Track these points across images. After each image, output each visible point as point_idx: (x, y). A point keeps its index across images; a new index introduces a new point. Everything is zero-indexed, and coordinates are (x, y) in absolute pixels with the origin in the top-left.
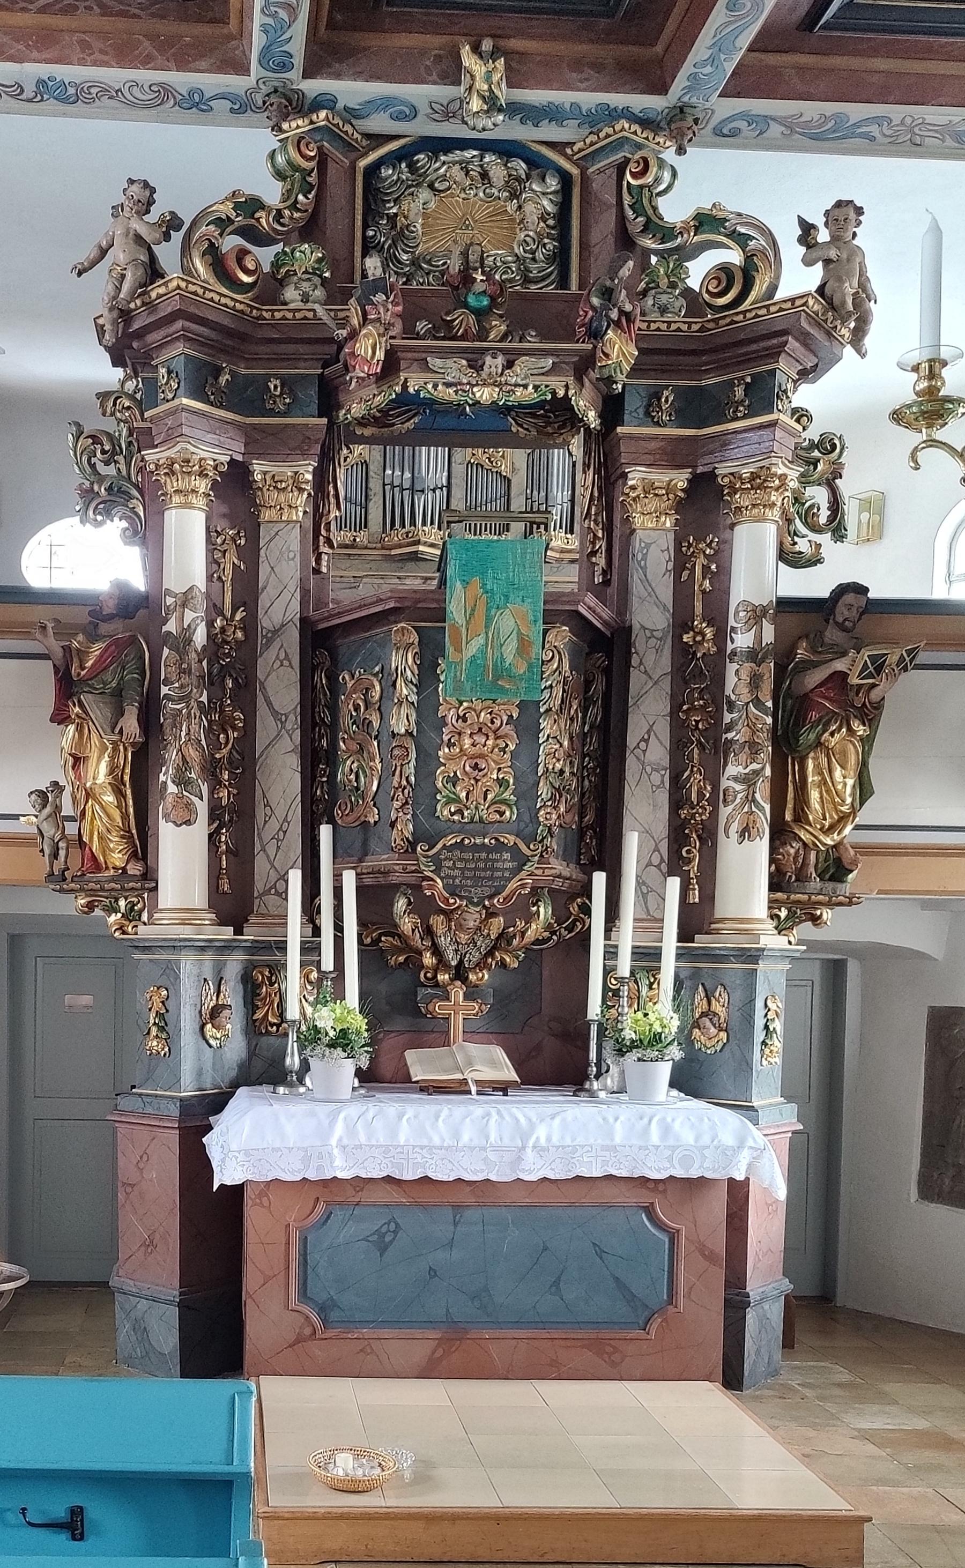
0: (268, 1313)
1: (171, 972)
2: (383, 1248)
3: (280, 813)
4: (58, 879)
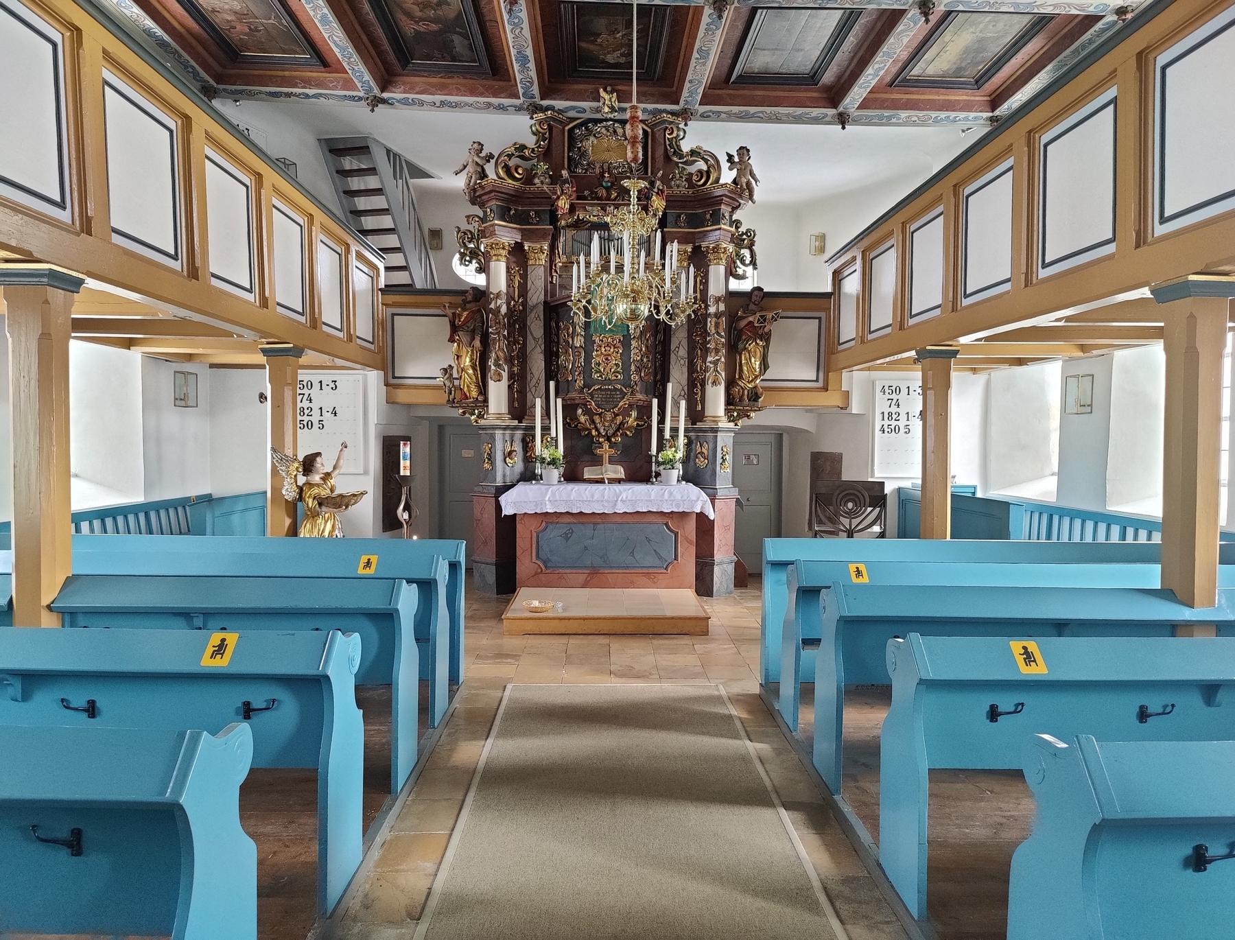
0: (525, 565)
1: (493, 437)
3: (536, 376)
4: (451, 403)
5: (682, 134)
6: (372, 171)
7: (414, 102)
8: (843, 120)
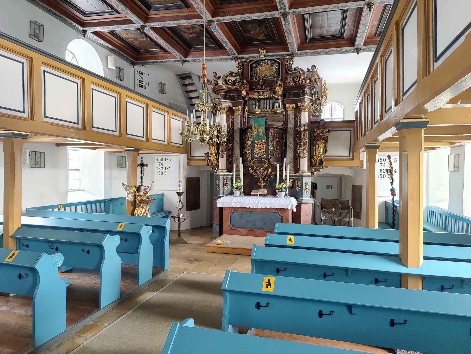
2: (241, 217)
3: (237, 156)
5: (292, 62)
6: (193, 84)
7: (196, 61)
8: (358, 50)
